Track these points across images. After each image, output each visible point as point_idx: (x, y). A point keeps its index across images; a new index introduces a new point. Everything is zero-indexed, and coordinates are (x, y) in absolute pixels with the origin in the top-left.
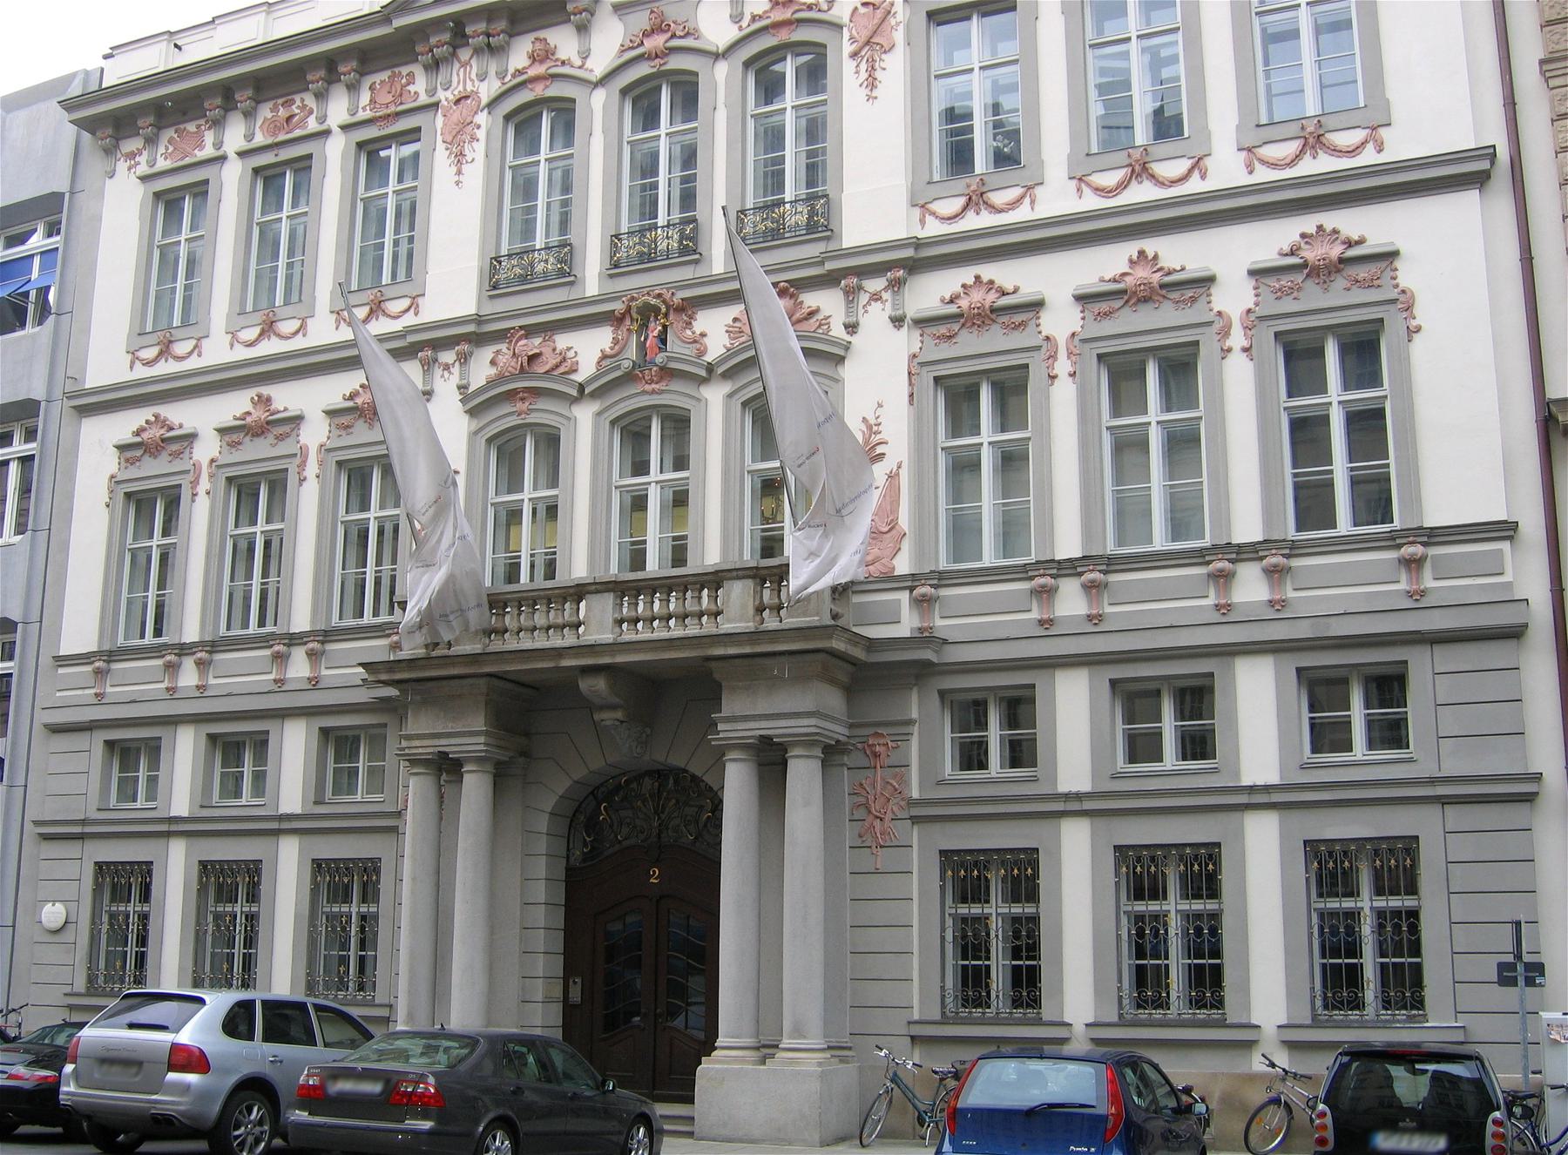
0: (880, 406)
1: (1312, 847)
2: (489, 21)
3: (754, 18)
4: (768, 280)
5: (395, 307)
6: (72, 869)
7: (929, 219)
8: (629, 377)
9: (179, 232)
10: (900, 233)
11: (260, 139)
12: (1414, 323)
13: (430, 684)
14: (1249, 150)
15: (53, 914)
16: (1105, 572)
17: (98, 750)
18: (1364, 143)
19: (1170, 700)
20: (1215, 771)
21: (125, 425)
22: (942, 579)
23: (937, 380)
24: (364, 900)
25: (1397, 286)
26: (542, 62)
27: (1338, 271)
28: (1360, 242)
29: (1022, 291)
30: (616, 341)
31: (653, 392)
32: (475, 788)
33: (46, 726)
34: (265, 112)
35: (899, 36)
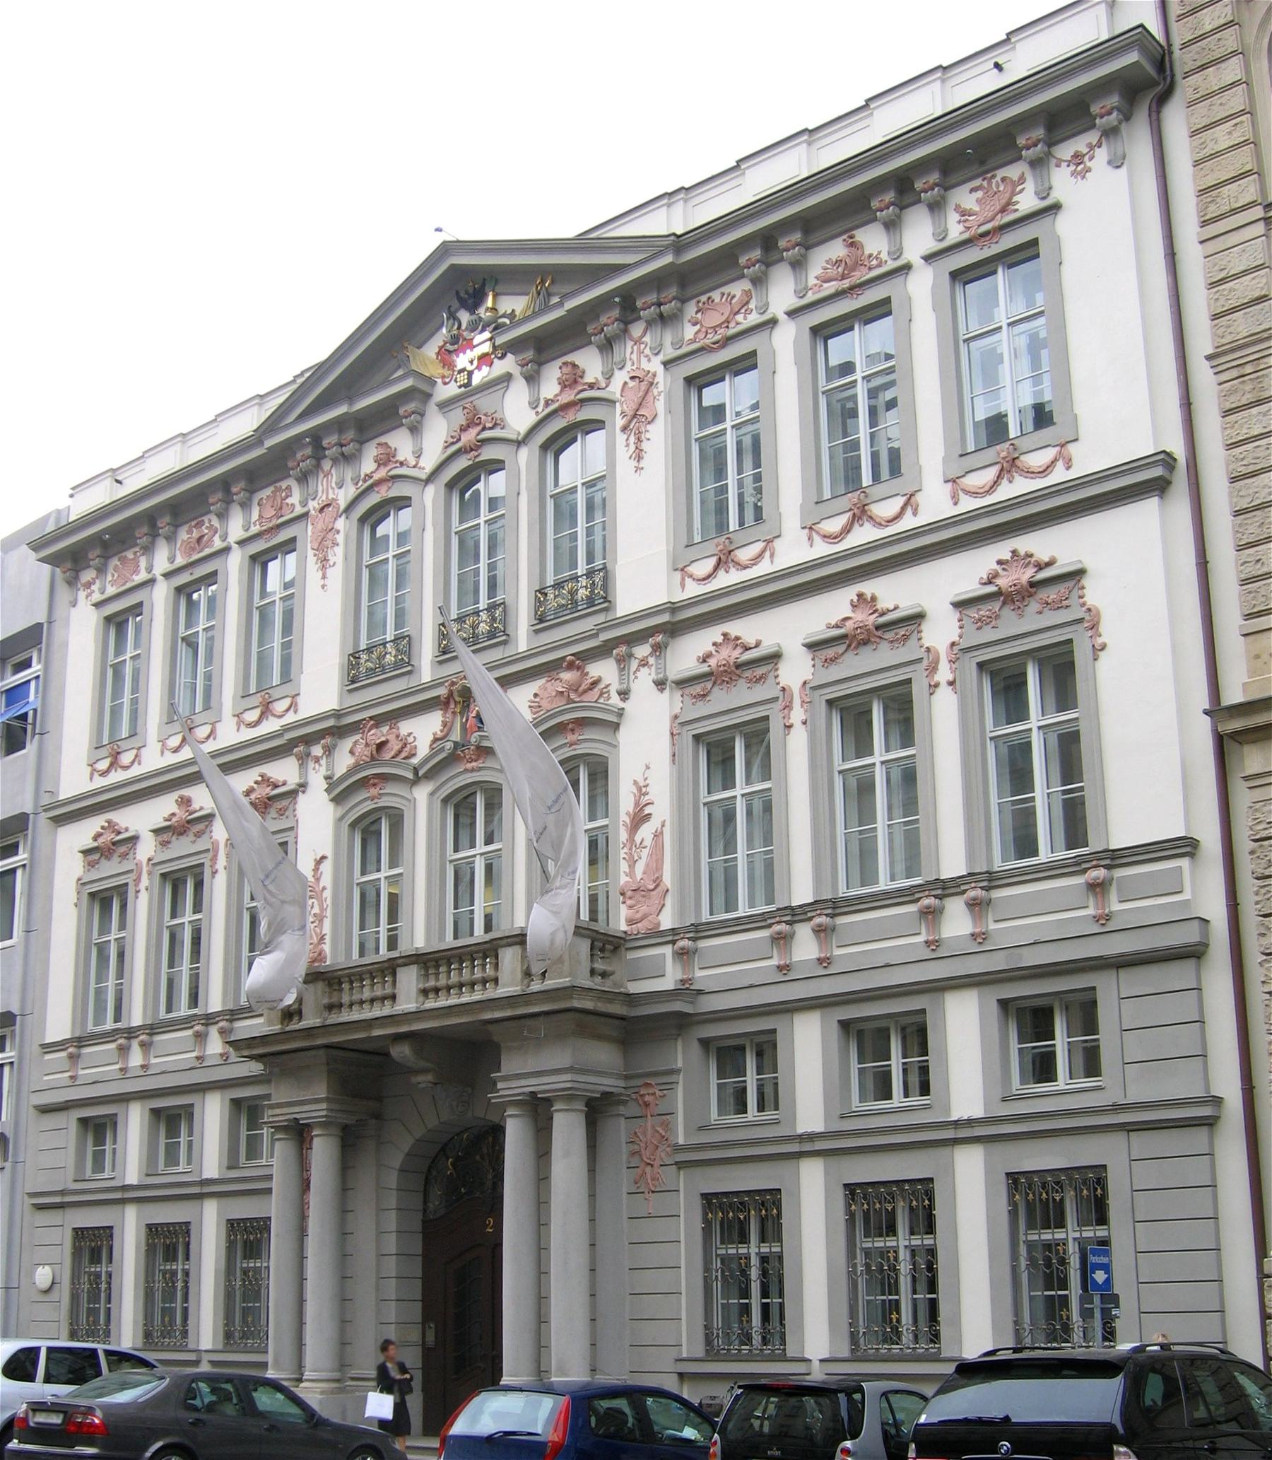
0: (648, 767)
1: (1014, 1180)
2: (659, 290)
3: (547, 403)
4: (491, 676)
5: (744, 555)
6: (55, 1236)
7: (688, 580)
8: (453, 758)
9: (387, 550)
10: (660, 598)
11: (180, 561)
12: (1100, 640)
13: (285, 1057)
14: (682, 570)
15: (43, 1276)
16: (987, 889)
17: (73, 1127)
18: (1053, 462)
19: (887, 1036)
20: (926, 1107)
21: (83, 833)
22: (699, 931)
23: (981, 666)
24: (763, 1239)
25: (1083, 605)
26: (385, 464)
27: (1031, 595)
28: (1049, 564)
29: (764, 644)
30: (445, 724)
31: (473, 770)
32: (323, 1151)
33: (36, 1107)
34: (183, 535)
35: (660, 406)
